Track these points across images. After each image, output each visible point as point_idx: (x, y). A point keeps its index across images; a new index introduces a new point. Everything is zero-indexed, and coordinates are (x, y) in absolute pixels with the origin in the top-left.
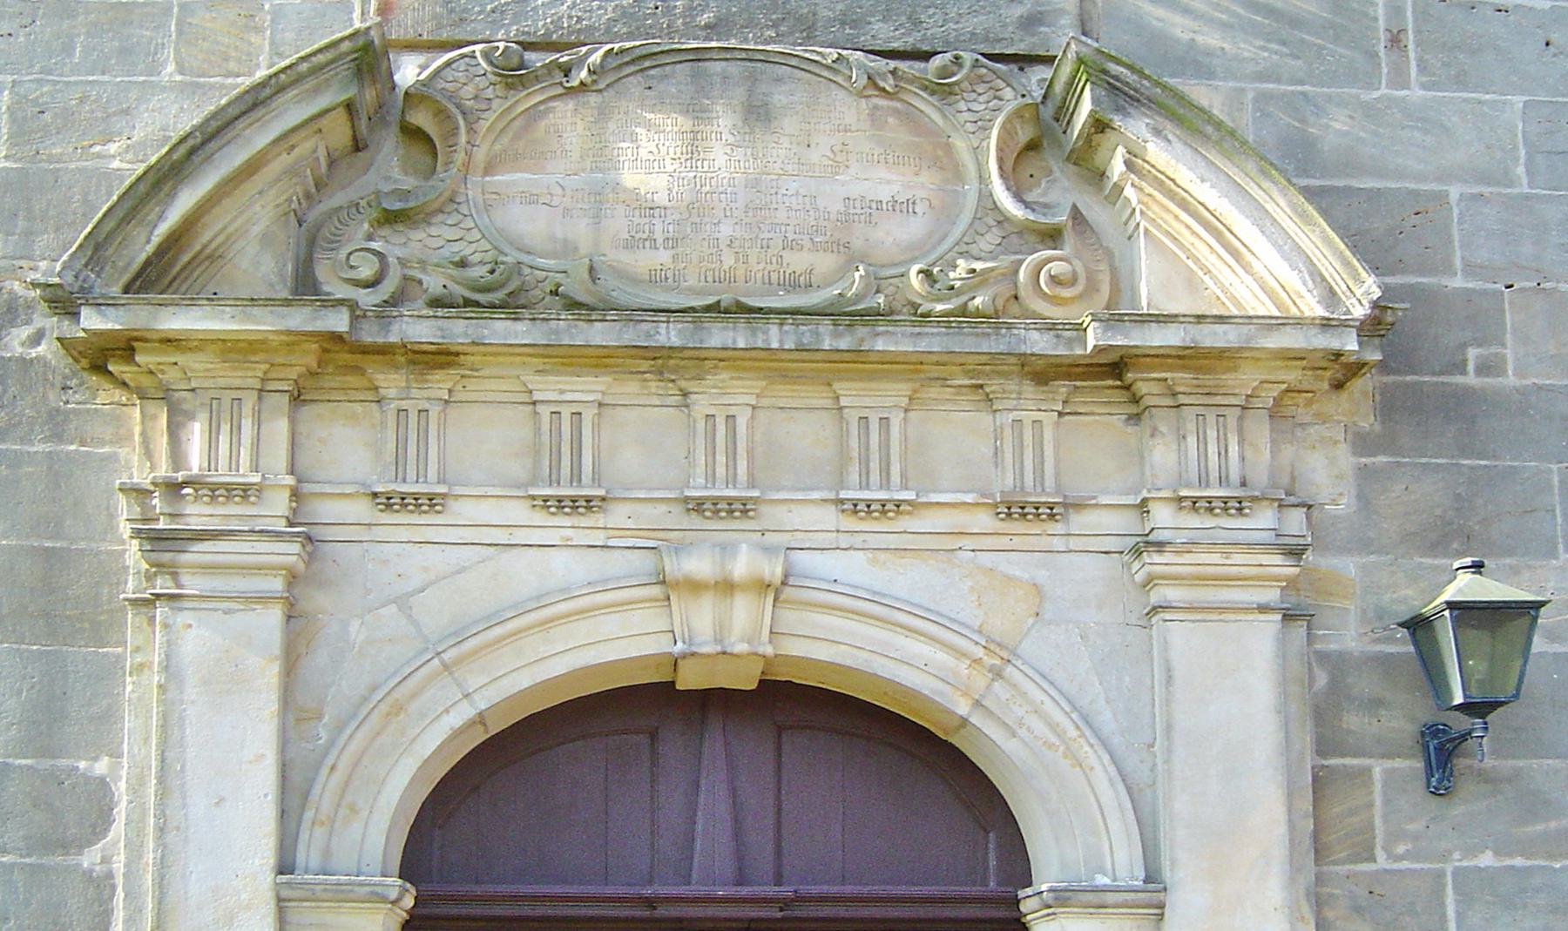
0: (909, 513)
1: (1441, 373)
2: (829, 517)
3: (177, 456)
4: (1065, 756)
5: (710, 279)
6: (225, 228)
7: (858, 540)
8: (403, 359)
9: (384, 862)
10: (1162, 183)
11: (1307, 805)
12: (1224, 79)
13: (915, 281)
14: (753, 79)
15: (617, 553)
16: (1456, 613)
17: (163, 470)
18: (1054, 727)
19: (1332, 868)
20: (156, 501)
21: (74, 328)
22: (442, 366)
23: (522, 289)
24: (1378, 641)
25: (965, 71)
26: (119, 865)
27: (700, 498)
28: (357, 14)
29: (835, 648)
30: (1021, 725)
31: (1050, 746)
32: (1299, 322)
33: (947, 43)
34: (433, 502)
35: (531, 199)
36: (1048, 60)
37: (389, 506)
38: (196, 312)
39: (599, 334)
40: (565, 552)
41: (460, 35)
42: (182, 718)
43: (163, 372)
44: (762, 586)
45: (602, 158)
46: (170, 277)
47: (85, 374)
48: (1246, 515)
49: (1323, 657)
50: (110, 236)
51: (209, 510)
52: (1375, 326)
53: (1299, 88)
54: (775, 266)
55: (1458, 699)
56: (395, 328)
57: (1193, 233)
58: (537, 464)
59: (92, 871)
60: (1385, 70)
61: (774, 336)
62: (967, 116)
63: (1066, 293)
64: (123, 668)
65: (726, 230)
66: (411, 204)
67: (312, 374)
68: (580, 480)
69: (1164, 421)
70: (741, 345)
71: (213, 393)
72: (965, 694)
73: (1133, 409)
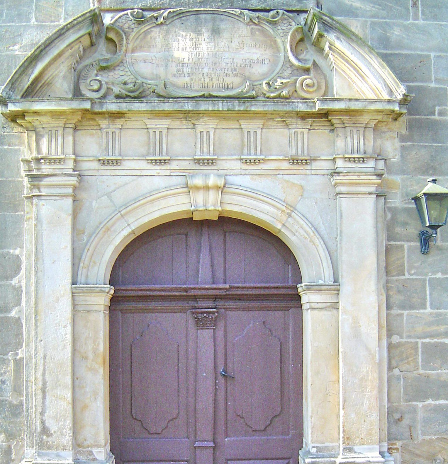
0: (263, 163)
1: (427, 115)
2: (238, 165)
3: (39, 150)
4: (310, 242)
5: (201, 86)
6: (52, 74)
7: (247, 172)
8: (107, 116)
9: (104, 280)
10: (340, 54)
11: (383, 257)
12: (361, 17)
13: (265, 87)
14: (214, 20)
15: (174, 177)
16: (426, 196)
17: (34, 155)
18: (306, 232)
19: (392, 278)
20: (32, 165)
21: (6, 109)
22: (120, 118)
23: (144, 91)
24: (406, 203)
25: (280, 16)
26: (23, 284)
27: (198, 159)
28: (91, 5)
29: (240, 207)
30: (297, 231)
31: (306, 238)
32: (381, 101)
33: (275, 6)
34: (117, 162)
35: (146, 61)
36: (306, 12)
37: (104, 164)
38: (44, 103)
39: (167, 107)
40: (158, 177)
41: (124, 7)
42: (42, 236)
43: (34, 122)
44: (218, 188)
45: (167, 47)
46: (35, 91)
47: (10, 123)
48: (365, 163)
49: (390, 209)
50: (17, 79)
51: (49, 167)
52: (404, 102)
53: (385, 20)
54: (221, 82)
55: (428, 224)
56: (105, 106)
57: (350, 70)
58: (149, 149)
59: (15, 286)
60: (411, 14)
61: (221, 106)
62: (281, 31)
63: (311, 90)
64: (23, 219)
65: (206, 70)
66: (109, 64)
67: (80, 121)
68: (162, 154)
69: (340, 132)
70: (210, 109)
71: (50, 129)
72: (280, 222)
73: (332, 128)
